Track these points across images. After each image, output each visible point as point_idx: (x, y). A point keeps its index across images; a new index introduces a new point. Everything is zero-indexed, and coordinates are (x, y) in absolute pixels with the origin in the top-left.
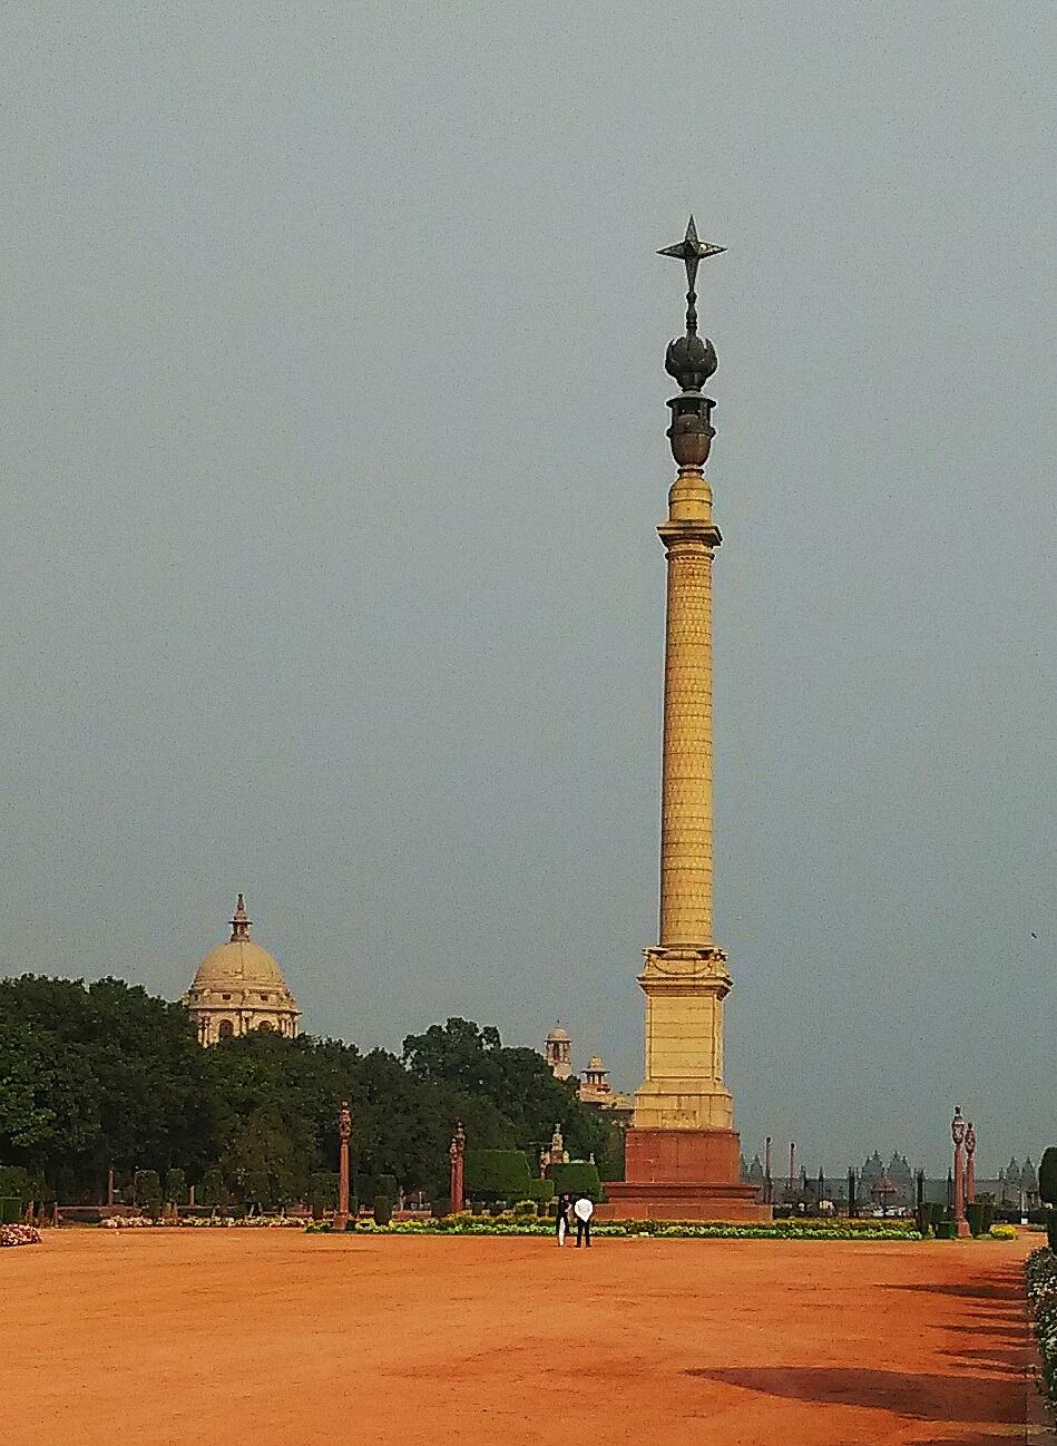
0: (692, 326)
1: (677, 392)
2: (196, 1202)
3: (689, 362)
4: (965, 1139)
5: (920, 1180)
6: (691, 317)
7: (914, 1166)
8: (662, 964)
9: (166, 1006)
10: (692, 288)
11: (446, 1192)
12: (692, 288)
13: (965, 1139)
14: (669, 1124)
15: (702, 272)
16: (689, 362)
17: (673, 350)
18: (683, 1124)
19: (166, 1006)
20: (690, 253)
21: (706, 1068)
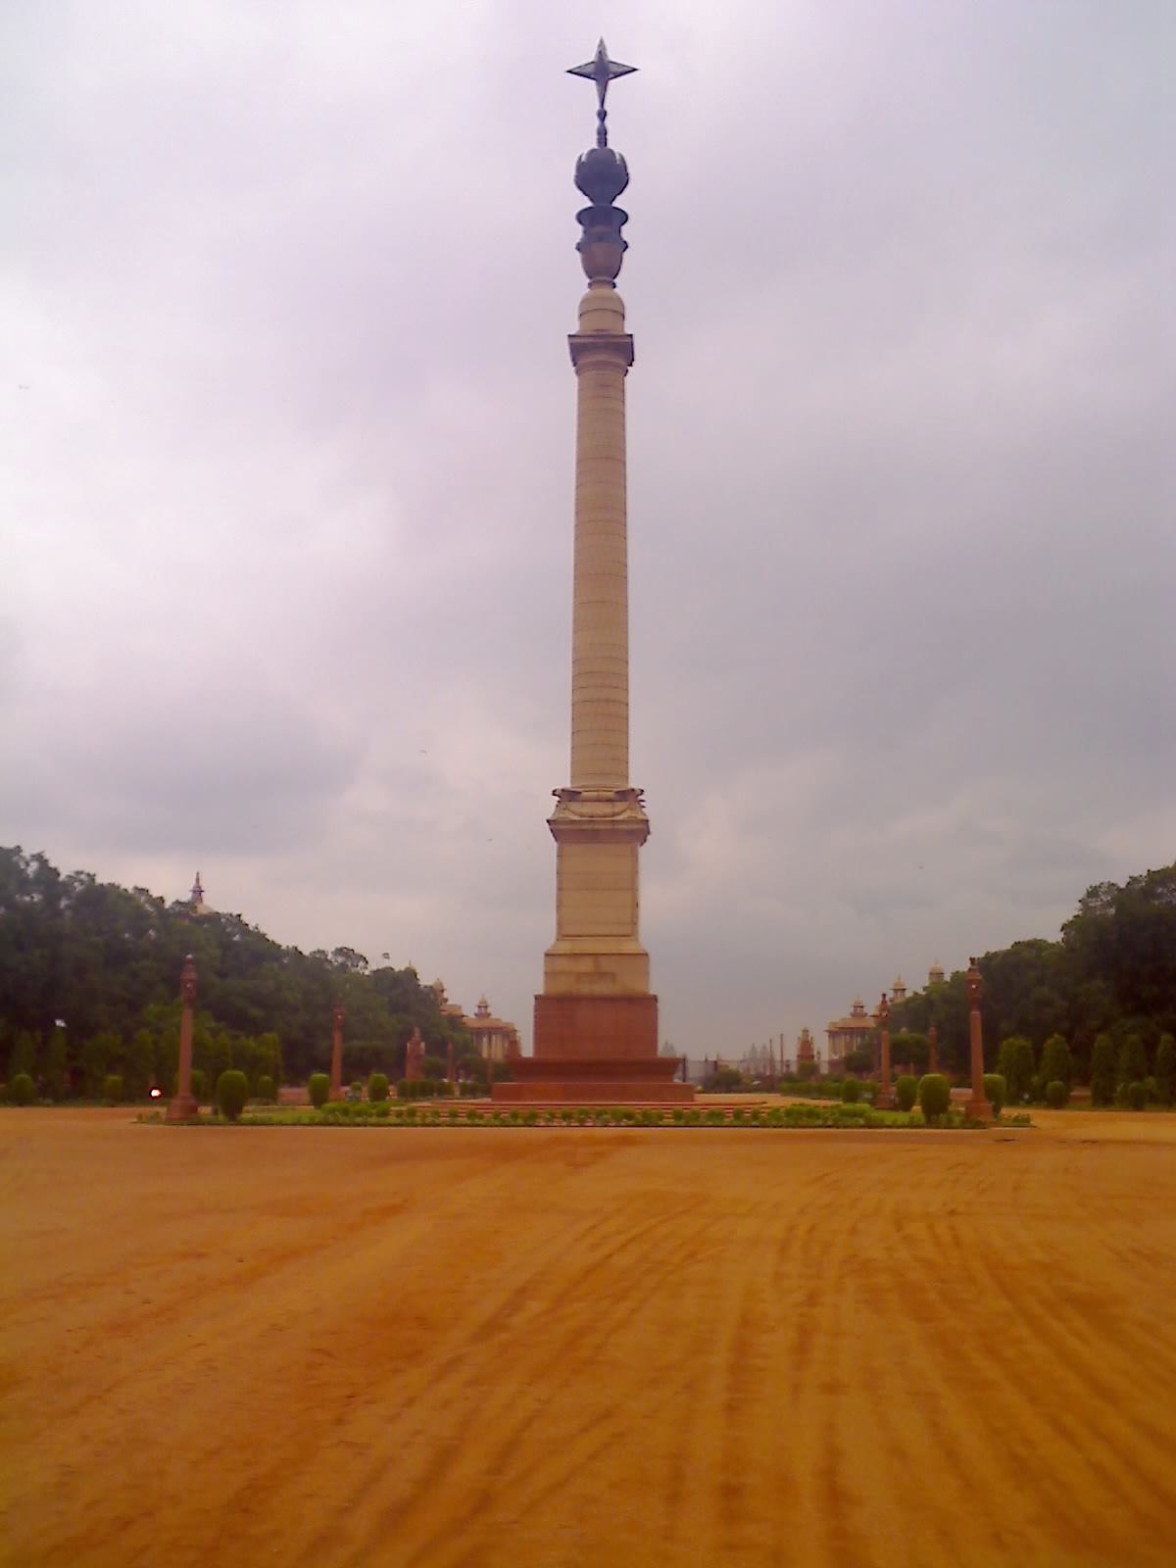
14: (586, 988)
18: (602, 988)
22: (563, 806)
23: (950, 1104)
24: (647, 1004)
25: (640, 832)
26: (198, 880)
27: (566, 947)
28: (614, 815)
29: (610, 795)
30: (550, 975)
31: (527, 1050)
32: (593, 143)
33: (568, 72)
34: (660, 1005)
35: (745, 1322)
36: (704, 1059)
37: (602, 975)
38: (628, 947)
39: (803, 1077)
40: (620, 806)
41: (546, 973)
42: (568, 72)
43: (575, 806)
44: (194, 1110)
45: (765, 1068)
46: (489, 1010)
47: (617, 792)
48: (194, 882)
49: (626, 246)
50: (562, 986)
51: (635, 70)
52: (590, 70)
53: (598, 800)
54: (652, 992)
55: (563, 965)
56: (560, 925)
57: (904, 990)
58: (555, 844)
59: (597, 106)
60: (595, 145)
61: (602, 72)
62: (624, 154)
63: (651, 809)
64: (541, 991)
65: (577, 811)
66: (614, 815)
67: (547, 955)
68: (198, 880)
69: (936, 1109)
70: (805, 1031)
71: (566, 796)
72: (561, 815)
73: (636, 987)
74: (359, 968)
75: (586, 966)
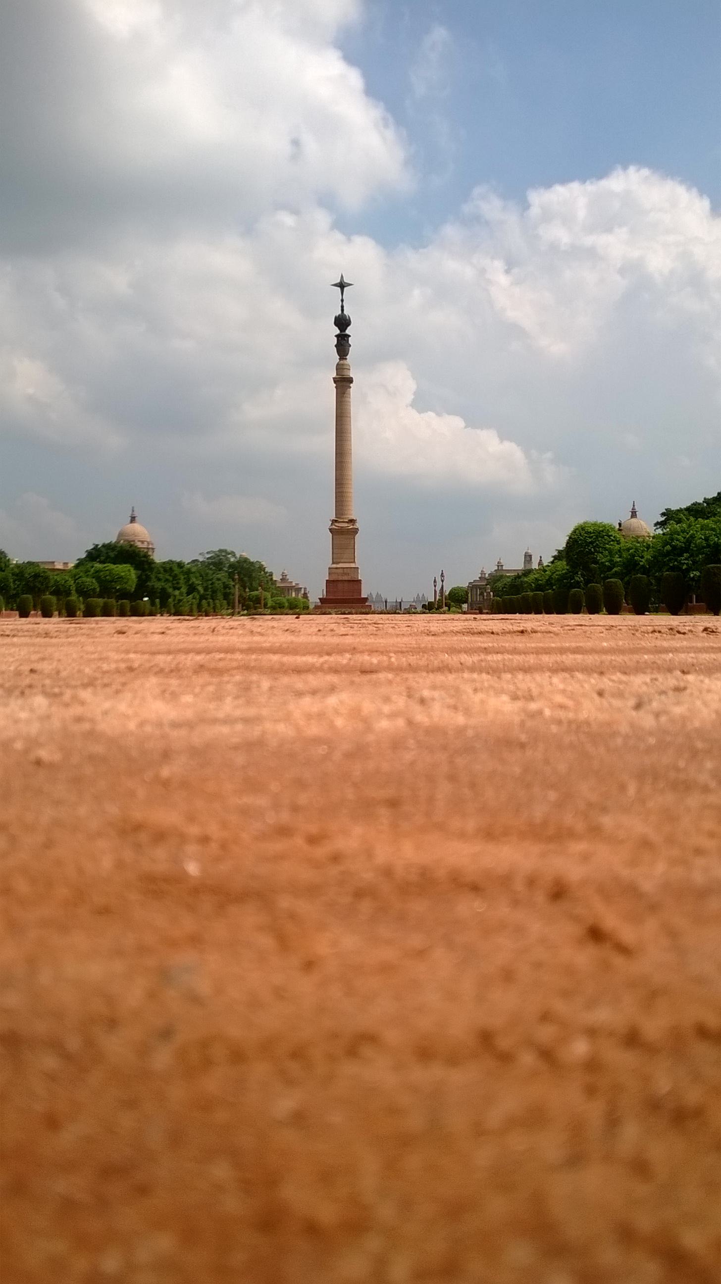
0: (342, 310)
1: (338, 332)
2: (696, 602)
3: (342, 322)
4: (528, 558)
5: (386, 602)
6: (342, 307)
7: (384, 598)
8: (337, 524)
9: (619, 741)
11: (234, 603)
13: (528, 558)
15: (334, 409)
16: (342, 322)
17: (336, 319)
18: (346, 578)
19: (619, 741)
20: (342, 285)
21: (352, 559)
24: (359, 582)
25: (356, 531)
26: (634, 506)
27: (334, 566)
28: (348, 527)
29: (347, 520)
31: (374, 600)
34: (362, 582)
36: (395, 601)
38: (353, 565)
44: (420, 653)
46: (288, 577)
48: (632, 506)
50: (334, 577)
52: (338, 285)
54: (359, 578)
58: (331, 534)
59: (341, 298)
60: (340, 312)
61: (342, 285)
62: (350, 315)
63: (357, 525)
64: (327, 579)
66: (348, 527)
68: (634, 506)
71: (334, 521)
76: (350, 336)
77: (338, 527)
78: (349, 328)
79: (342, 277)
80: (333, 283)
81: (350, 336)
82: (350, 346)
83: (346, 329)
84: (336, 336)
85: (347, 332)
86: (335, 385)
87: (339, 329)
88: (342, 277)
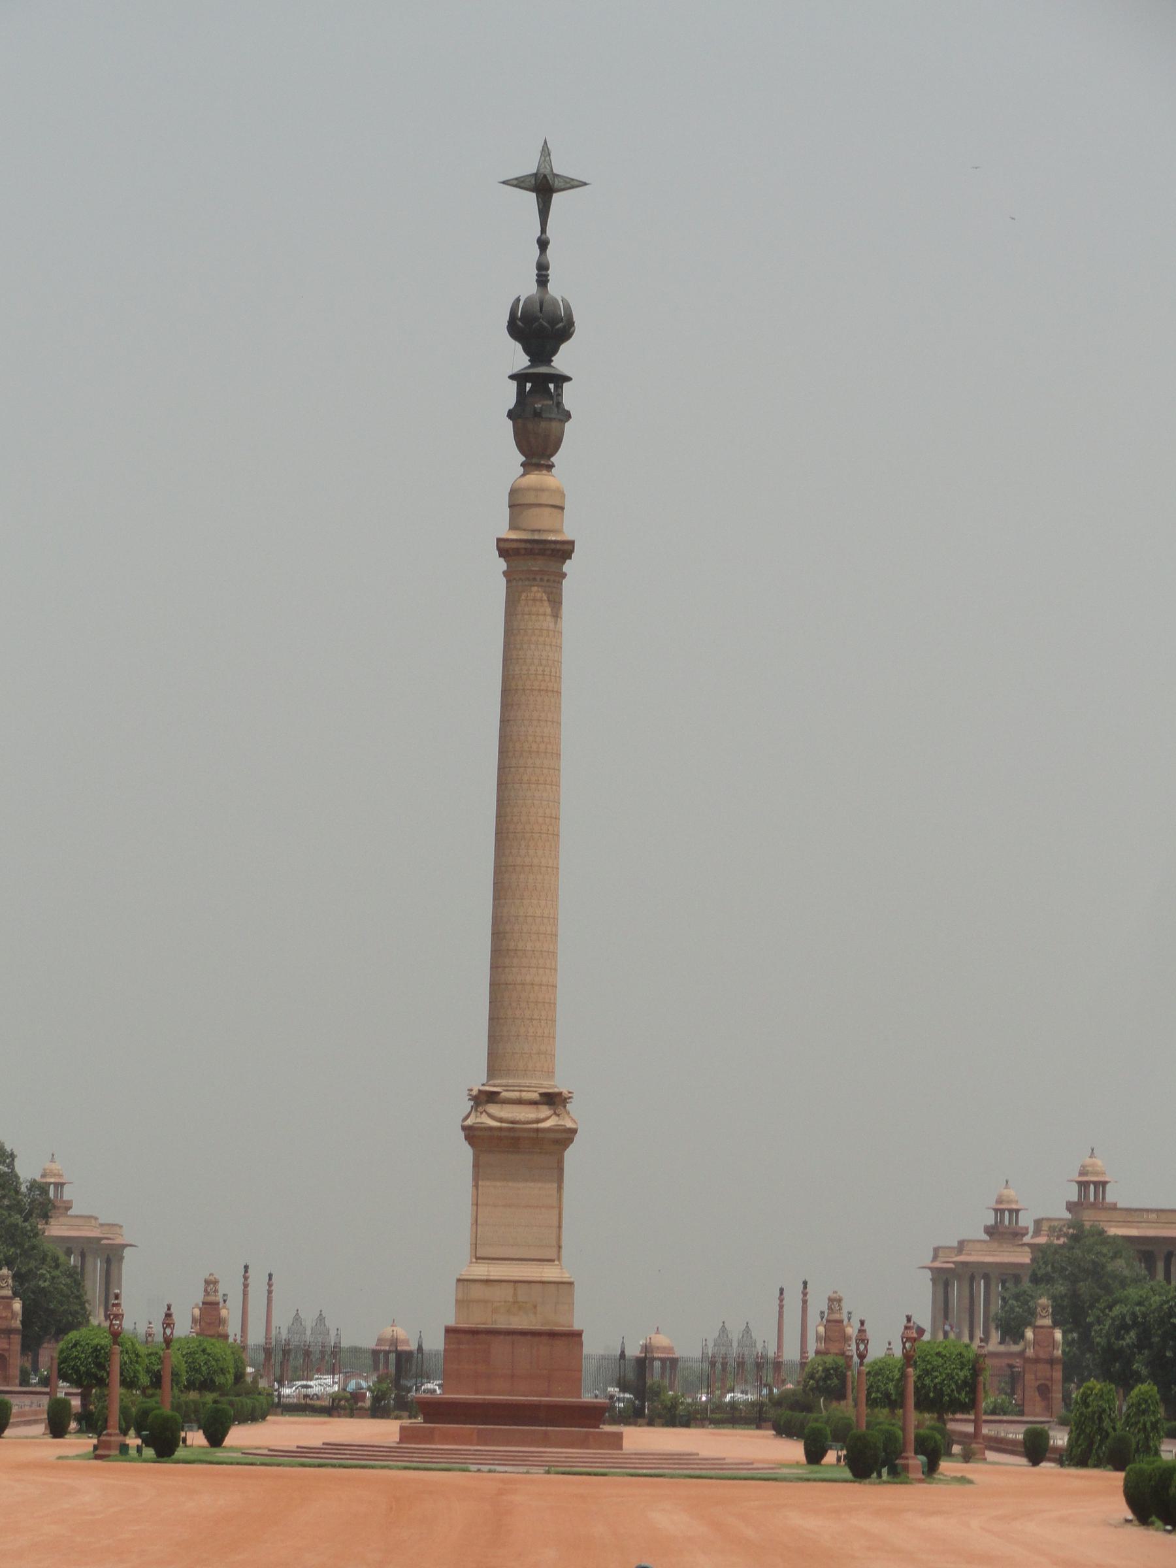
6: (542, 269)
10: (543, 230)
12: (543, 230)
14: (503, 1322)
22: (480, 1109)
23: (77, 1330)
30: (461, 1303)
32: (528, 288)
33: (504, 183)
35: (743, 1355)
37: (517, 1306)
39: (74, 1457)
40: (545, 1111)
41: (457, 1301)
42: (504, 183)
43: (493, 1109)
45: (83, 1340)
47: (541, 1094)
49: (568, 416)
50: (478, 1319)
51: (585, 184)
53: (520, 1102)
54: (577, 1327)
55: (477, 1292)
56: (475, 1246)
57: (1104, 1184)
59: (537, 233)
63: (576, 1115)
64: (451, 1322)
65: (492, 1117)
66: (538, 1121)
67: (459, 1280)
69: (83, 1286)
70: (520, 296)
71: (484, 1099)
72: (479, 1120)
73: (559, 1323)
74: (1112, 1434)
75: (505, 1293)
76: (568, 379)
77: (501, 1120)
78: (564, 348)
79: (546, 151)
80: (587, 186)
81: (568, 379)
82: (568, 416)
83: (555, 351)
84: (512, 377)
85: (562, 361)
86: (502, 565)
87: (527, 350)
88: (546, 151)
